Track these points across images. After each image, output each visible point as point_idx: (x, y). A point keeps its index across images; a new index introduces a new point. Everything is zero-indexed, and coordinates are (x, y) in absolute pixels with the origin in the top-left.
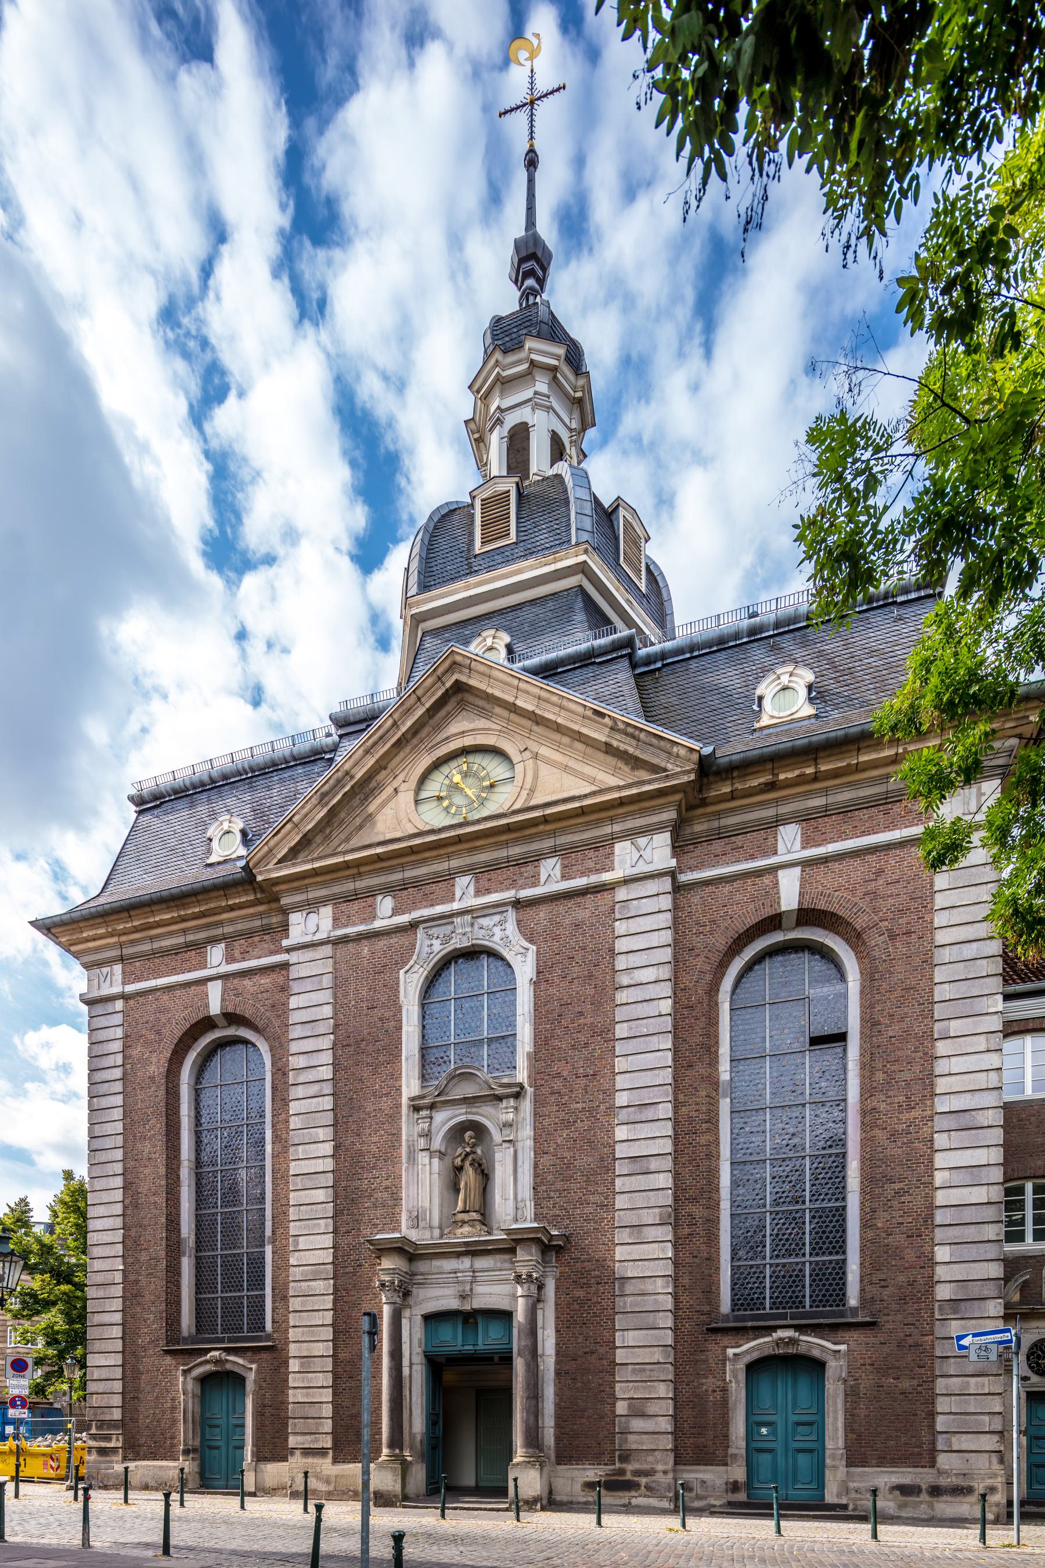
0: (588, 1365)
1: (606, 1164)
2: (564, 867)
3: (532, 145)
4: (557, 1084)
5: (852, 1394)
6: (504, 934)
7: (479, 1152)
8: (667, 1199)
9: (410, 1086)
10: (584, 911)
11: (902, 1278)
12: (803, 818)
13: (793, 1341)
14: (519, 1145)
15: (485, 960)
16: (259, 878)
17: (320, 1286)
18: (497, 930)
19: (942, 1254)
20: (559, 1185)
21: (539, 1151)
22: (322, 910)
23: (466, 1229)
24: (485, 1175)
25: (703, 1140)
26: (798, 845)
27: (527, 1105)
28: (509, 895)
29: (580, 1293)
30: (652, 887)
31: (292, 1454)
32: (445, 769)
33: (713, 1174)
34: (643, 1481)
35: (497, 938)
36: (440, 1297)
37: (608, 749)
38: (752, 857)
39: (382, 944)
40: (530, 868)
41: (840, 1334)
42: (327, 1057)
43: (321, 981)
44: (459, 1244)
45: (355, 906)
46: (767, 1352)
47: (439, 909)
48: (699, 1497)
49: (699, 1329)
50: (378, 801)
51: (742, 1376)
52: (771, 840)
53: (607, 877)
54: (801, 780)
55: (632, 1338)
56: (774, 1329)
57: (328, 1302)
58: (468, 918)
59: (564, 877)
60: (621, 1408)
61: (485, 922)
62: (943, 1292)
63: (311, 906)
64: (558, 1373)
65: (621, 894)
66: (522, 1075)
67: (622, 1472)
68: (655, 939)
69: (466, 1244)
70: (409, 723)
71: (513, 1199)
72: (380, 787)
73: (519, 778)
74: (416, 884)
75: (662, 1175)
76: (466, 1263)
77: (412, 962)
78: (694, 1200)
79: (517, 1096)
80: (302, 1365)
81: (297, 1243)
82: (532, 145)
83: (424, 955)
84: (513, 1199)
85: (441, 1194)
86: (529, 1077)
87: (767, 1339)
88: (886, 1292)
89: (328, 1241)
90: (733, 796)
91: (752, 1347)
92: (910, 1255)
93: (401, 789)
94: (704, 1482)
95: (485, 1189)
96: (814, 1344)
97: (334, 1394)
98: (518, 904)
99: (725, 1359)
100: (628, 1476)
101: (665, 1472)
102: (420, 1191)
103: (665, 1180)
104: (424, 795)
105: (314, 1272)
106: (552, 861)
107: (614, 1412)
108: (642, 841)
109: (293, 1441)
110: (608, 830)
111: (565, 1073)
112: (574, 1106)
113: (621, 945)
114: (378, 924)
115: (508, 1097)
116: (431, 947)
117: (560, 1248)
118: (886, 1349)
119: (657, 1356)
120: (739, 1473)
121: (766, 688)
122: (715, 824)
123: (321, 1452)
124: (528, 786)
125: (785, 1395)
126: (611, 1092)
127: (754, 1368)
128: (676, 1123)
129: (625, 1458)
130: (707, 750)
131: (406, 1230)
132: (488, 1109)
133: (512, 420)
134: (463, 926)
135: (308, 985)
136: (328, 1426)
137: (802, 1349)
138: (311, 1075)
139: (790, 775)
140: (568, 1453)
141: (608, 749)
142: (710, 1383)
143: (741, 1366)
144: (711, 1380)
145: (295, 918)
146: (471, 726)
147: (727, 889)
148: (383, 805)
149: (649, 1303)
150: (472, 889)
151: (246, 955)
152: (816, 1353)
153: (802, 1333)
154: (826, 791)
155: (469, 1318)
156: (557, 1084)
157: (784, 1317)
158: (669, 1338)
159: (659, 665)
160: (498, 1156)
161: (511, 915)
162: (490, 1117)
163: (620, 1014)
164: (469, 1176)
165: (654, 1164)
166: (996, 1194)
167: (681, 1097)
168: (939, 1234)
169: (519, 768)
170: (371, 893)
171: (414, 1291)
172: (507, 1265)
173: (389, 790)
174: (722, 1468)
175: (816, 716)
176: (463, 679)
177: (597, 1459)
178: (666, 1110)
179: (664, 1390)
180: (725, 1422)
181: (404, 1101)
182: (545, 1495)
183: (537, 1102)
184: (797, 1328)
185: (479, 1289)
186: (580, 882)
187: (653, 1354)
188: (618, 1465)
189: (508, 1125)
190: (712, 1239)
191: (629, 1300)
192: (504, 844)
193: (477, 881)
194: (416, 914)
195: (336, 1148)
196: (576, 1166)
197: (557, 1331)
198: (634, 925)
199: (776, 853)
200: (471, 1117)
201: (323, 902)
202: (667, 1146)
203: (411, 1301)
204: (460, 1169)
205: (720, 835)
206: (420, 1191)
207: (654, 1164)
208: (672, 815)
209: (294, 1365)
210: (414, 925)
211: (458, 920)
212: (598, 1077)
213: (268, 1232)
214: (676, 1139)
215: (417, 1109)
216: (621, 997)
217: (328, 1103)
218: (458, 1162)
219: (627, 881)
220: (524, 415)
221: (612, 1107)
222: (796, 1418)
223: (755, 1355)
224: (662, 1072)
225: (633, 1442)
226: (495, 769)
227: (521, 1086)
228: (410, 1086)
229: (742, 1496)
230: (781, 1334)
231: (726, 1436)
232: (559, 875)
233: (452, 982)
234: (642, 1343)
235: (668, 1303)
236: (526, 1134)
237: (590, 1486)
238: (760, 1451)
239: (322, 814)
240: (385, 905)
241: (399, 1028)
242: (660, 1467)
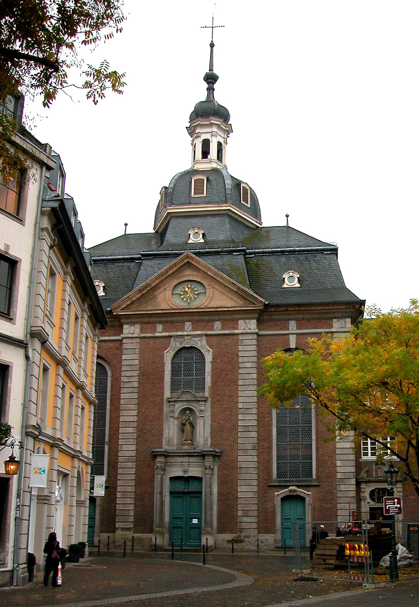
0: (228, 498)
1: (235, 427)
2: (222, 325)
3: (212, 41)
4: (219, 398)
5: (313, 508)
6: (201, 344)
7: (191, 419)
8: (255, 441)
9: (167, 393)
10: (228, 341)
11: (327, 471)
12: (297, 320)
13: (295, 491)
14: (206, 418)
15: (194, 350)
16: (114, 314)
17: (130, 465)
18: (199, 342)
19: (338, 463)
20: (219, 433)
21: (213, 421)
22: (136, 325)
23: (186, 447)
24: (193, 426)
25: (267, 419)
26: (295, 328)
27: (209, 404)
28: (204, 332)
29: (226, 472)
30: (250, 337)
31: (117, 530)
32: (183, 285)
33: (271, 431)
34: (247, 539)
35: (199, 345)
36: (178, 472)
37: (236, 292)
38: (281, 329)
39: (158, 341)
40: (211, 323)
41: (309, 488)
42: (136, 379)
43: (135, 351)
44: (184, 453)
45: (149, 326)
46: (288, 494)
47: (179, 333)
48: (265, 545)
49: (266, 486)
50: (159, 291)
51: (280, 502)
52: (287, 325)
53: (236, 331)
54: (295, 310)
55: (244, 488)
56: (289, 486)
57: (133, 471)
58: (189, 337)
59: (223, 329)
60: (240, 513)
61: (195, 339)
62: (339, 476)
63: (132, 324)
64: (218, 500)
65: (241, 337)
66: (207, 394)
67: (240, 536)
68: (251, 354)
69: (187, 453)
70: (171, 272)
71: (203, 435)
72: (159, 288)
73: (207, 294)
74: (171, 322)
75: (253, 433)
76: (186, 459)
77: (169, 349)
78: (264, 440)
79: (205, 401)
80: (122, 495)
81: (122, 448)
82: (212, 41)
83: (173, 347)
84: (203, 435)
85: (177, 434)
86: (209, 395)
87: (287, 490)
88: (323, 475)
89: (134, 447)
90: (275, 311)
91: (283, 492)
92: (329, 463)
93: (167, 289)
94: (267, 540)
95: (193, 432)
96: (301, 491)
97: (135, 507)
98: (207, 335)
99: (274, 496)
100: (242, 538)
101: (254, 536)
102: (171, 431)
103: (254, 434)
104: (175, 292)
105: (128, 459)
106: (218, 323)
107: (237, 515)
108: (247, 321)
109: (118, 525)
110: (237, 316)
111: (222, 394)
112: (224, 406)
113: (241, 354)
114: (157, 334)
115: (202, 401)
116: (175, 345)
117: (219, 455)
118: (323, 494)
119: (251, 495)
120: (279, 536)
121: (286, 276)
122: (270, 317)
123: (129, 529)
124: (211, 297)
125: (293, 510)
126: (237, 403)
127: (284, 499)
128: (258, 414)
129: (241, 532)
130: (267, 303)
131: (165, 447)
132: (195, 404)
133: (204, 137)
134: (188, 340)
135: (130, 352)
136: (132, 519)
137: (298, 493)
138: (130, 385)
139: (292, 309)
140: (221, 530)
141: (236, 292)
142: (269, 504)
143: (279, 499)
144: (269, 503)
145: (125, 326)
146: (192, 273)
147: (274, 337)
148: (160, 293)
149: (249, 476)
150: (191, 328)
151: (104, 334)
152: (302, 495)
153: (298, 488)
154: (303, 314)
155: (187, 480)
156: (219, 398)
157: (293, 481)
158: (255, 489)
159: (253, 256)
160: (198, 421)
161: (204, 338)
162: (194, 406)
163: (240, 377)
164: (188, 427)
165: (251, 429)
166: (353, 445)
167: (260, 404)
168: (338, 457)
169: (208, 291)
170: (155, 323)
171: (167, 468)
172: (201, 461)
173: (163, 289)
174: (273, 535)
175: (300, 287)
176: (190, 261)
177: (232, 532)
178: (255, 411)
179: (254, 507)
180: (274, 518)
181: (165, 398)
182: (213, 545)
183: (213, 403)
184: (297, 486)
185: (191, 469)
186: (228, 332)
187: (254, 458)
188: (239, 534)
189: (201, 411)
190: (270, 454)
191: (243, 475)
192: (203, 317)
193: (193, 325)
194: (171, 334)
195: (138, 412)
196: (226, 426)
197: (218, 485)
198: (245, 348)
199: (288, 329)
200: (189, 406)
201: (137, 323)
202: (255, 423)
203: (166, 472)
204: (184, 424)
205: (271, 320)
206: (171, 431)
207: (251, 429)
208: (257, 316)
209: (119, 495)
210: (170, 337)
211: (186, 338)
212: (233, 397)
213: (107, 439)
214: (258, 420)
215: (169, 402)
216: (241, 371)
217: (136, 396)
218: (184, 422)
219: (242, 334)
220: (208, 136)
221: (237, 408)
222: (297, 517)
223: (283, 495)
224: (254, 398)
225: (244, 525)
226: (200, 289)
227: (207, 398)
228: (167, 393)
229: (280, 545)
230: (291, 488)
231: (275, 523)
232: (220, 328)
233: (183, 354)
234: (247, 490)
235: (256, 477)
236: (208, 414)
237: (229, 541)
238: (286, 528)
239: (139, 296)
240: (160, 327)
241: (164, 371)
242: (252, 535)
